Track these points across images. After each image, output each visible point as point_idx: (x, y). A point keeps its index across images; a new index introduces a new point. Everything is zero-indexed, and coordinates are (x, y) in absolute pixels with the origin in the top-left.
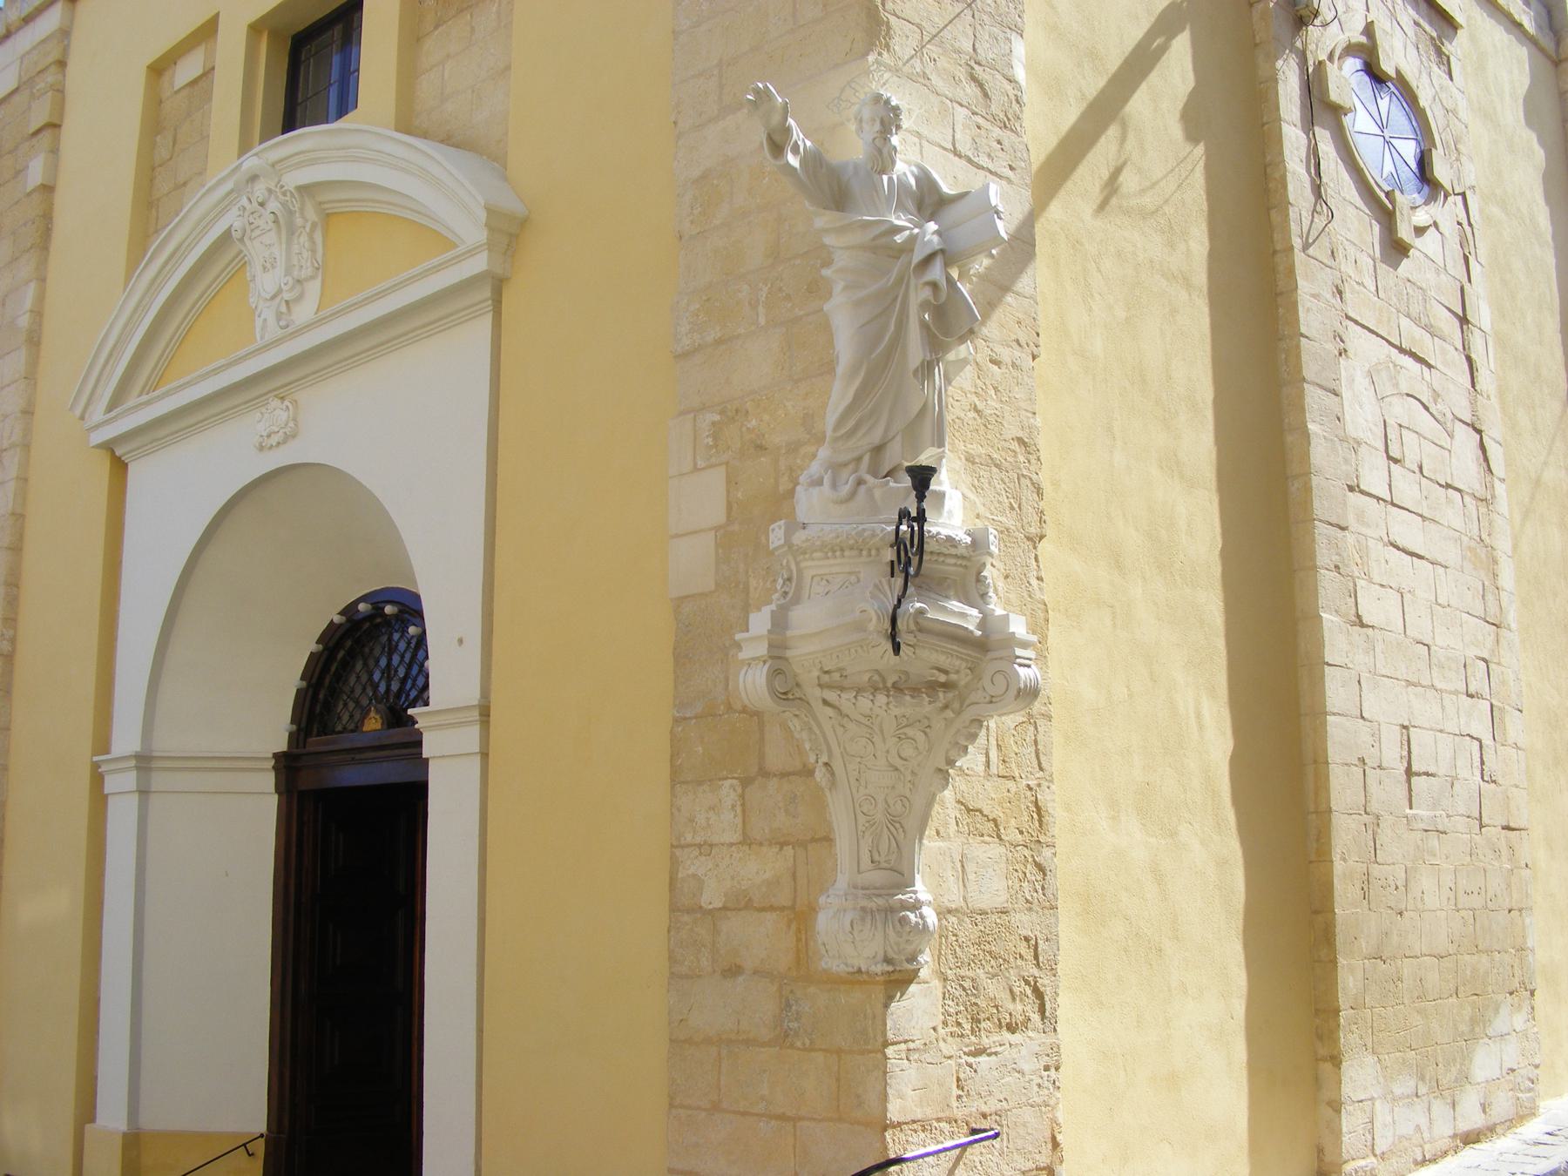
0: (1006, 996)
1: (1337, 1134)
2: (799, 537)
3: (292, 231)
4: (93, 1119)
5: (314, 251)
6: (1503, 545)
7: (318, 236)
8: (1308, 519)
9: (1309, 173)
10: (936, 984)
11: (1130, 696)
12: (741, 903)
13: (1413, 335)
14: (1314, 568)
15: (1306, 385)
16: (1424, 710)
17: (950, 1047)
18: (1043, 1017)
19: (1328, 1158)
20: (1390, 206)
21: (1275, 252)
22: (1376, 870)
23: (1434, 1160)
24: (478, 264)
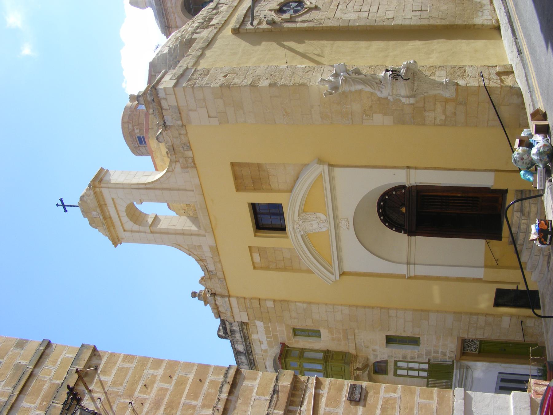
0: (460, 72)
1: (488, 25)
2: (391, 94)
4: (482, 279)
5: (311, 214)
7: (308, 213)
9: (306, 23)
10: (458, 80)
11: (409, 55)
12: (444, 112)
15: (349, 25)
17: (468, 79)
18: (464, 67)
19: (492, 27)
20: (308, 8)
21: (323, 29)
23: (495, 9)
24: (326, 167)
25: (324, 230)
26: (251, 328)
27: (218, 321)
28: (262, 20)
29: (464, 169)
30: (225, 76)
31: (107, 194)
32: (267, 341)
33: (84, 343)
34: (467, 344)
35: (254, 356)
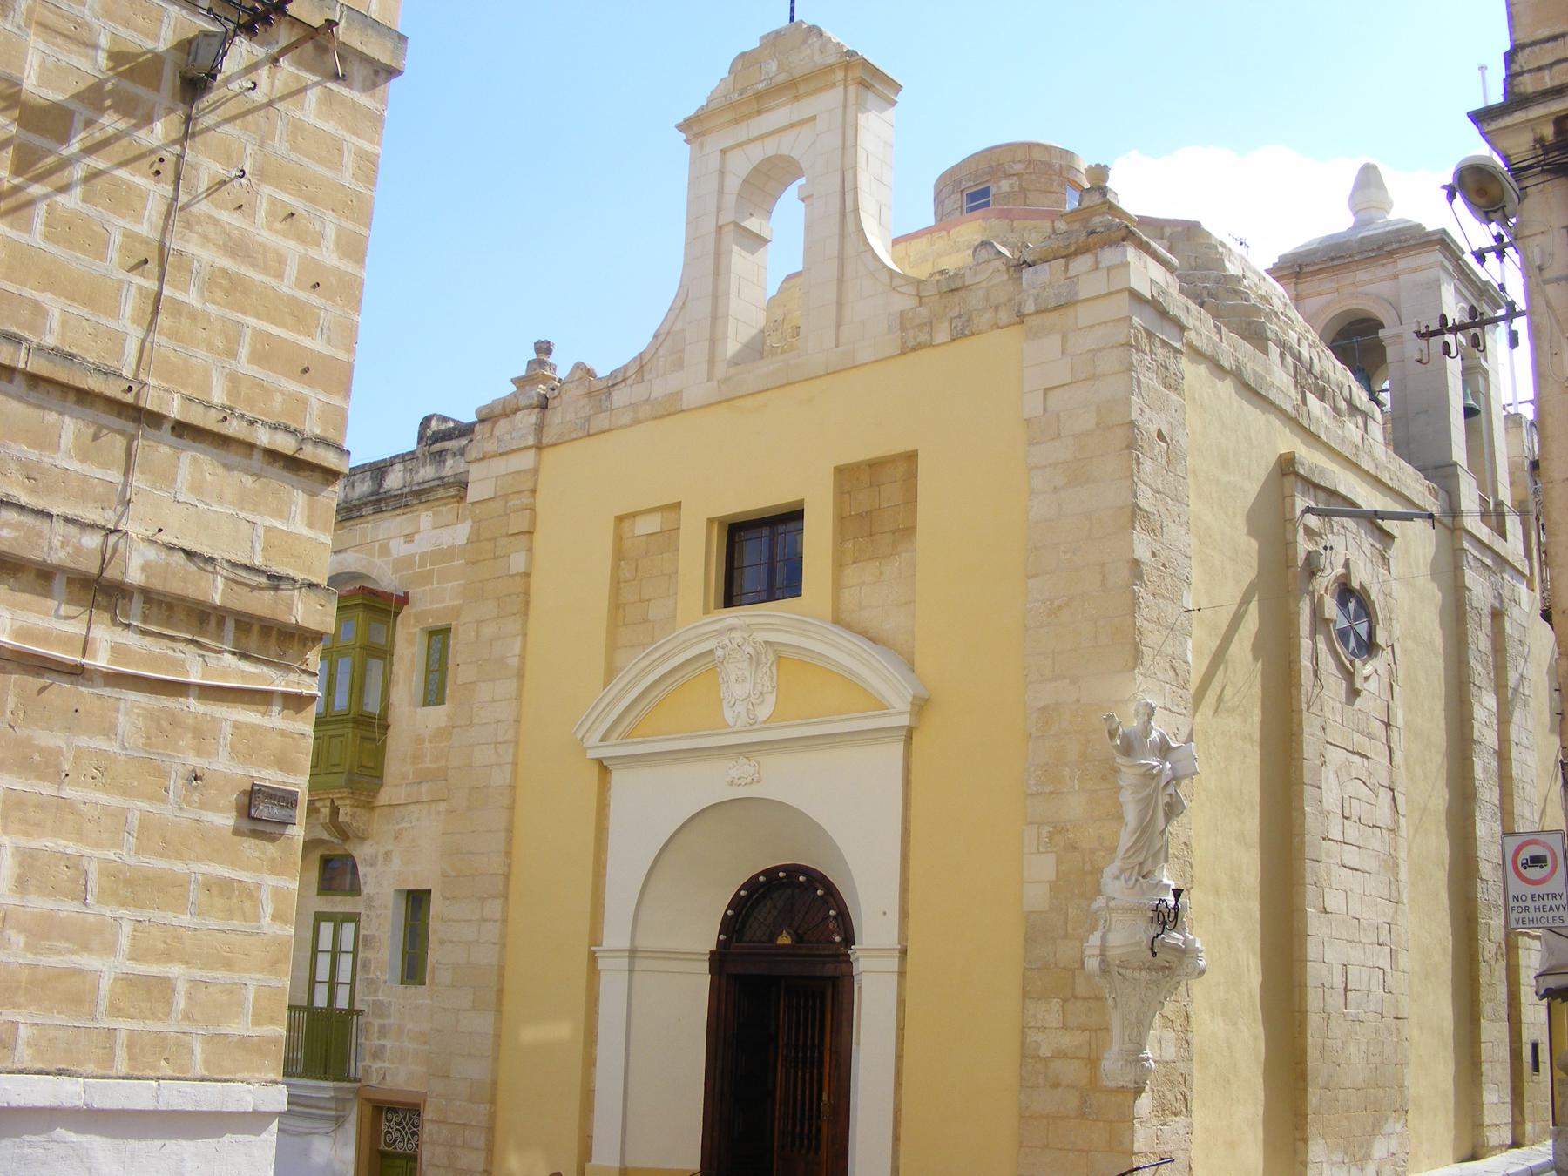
3: (758, 665)
4: (590, 1161)
5: (772, 678)
6: (1402, 854)
7: (774, 669)
8: (1302, 858)
12: (1061, 1055)
13: (1360, 741)
14: (1304, 884)
16: (1355, 955)
17: (1154, 1121)
21: (1292, 711)
22: (1328, 1042)
24: (905, 720)
25: (729, 716)
26: (448, 511)
27: (468, 417)
28: (1318, 539)
29: (900, 1110)
30: (1161, 436)
31: (826, 102)
32: (414, 555)
33: (409, 41)
34: (405, 1118)
35: (370, 518)
